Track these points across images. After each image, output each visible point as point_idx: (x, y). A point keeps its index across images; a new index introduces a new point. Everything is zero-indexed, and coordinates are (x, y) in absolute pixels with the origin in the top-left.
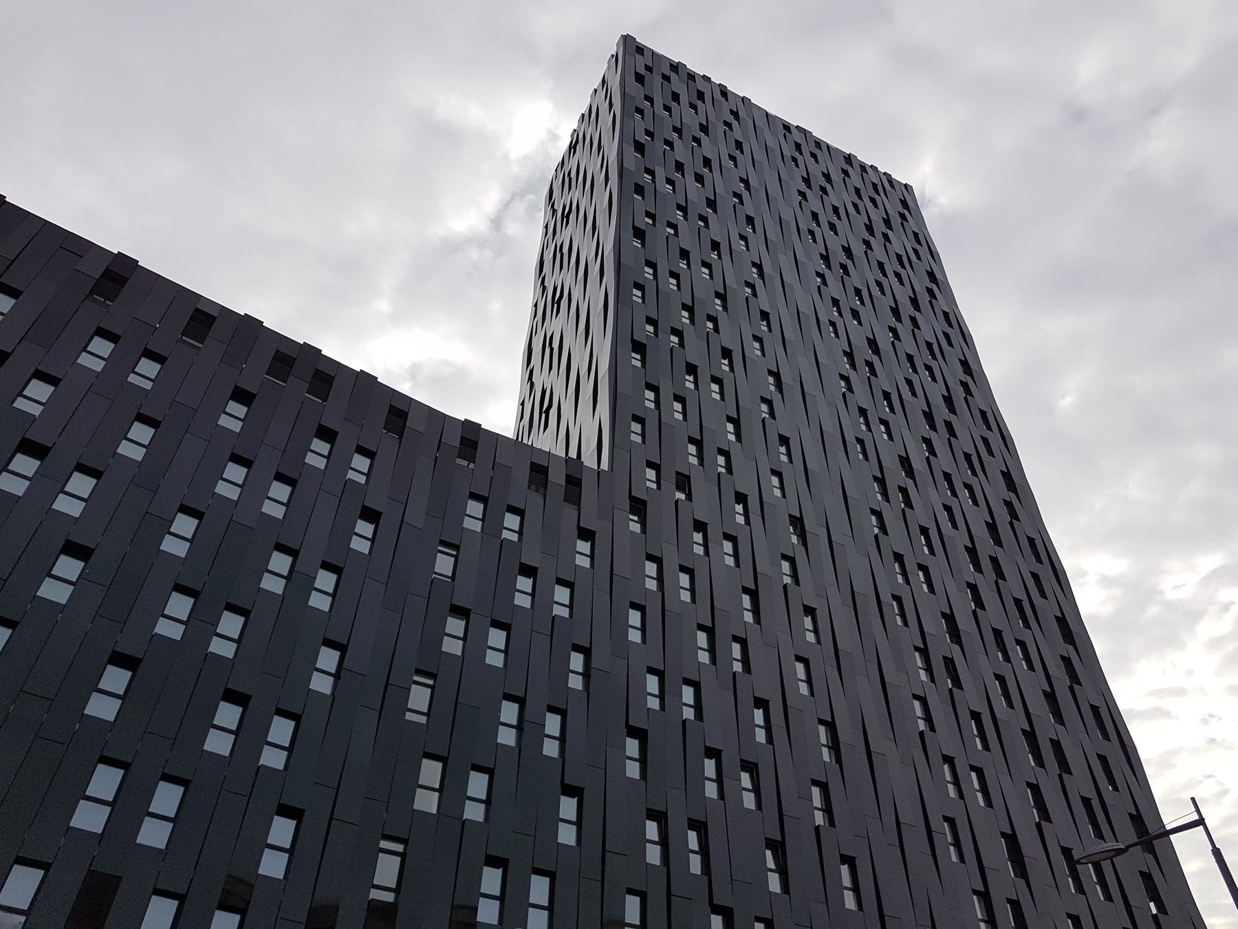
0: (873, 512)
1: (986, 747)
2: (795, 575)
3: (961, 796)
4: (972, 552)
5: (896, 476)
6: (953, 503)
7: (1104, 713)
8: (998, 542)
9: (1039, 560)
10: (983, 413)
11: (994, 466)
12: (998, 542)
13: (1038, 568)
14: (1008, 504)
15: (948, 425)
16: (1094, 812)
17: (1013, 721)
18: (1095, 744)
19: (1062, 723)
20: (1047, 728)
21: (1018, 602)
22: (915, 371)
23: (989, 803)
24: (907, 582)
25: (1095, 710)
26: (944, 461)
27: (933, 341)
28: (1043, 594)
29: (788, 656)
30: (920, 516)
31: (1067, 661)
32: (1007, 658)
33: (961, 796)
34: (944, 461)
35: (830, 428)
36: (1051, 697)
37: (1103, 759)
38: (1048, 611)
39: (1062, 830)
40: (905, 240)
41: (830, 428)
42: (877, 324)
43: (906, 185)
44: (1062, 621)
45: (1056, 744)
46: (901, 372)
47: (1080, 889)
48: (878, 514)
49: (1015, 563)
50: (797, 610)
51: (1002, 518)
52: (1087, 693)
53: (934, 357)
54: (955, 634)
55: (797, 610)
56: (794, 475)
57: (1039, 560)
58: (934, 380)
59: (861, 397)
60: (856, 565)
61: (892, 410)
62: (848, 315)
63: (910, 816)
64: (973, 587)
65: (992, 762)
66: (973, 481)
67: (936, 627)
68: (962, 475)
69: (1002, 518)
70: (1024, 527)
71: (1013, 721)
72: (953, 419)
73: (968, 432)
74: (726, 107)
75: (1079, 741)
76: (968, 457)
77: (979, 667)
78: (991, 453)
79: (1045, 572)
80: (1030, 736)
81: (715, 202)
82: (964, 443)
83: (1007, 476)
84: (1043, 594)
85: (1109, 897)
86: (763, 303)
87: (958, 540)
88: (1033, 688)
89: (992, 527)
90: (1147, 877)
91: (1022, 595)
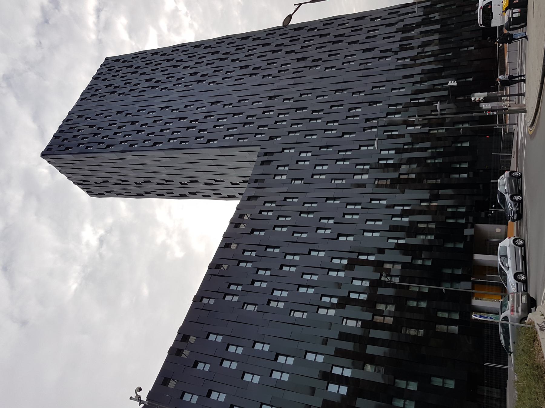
0: (161, 90)
3: (353, 61)
4: (133, 73)
6: (120, 76)
7: (218, 41)
9: (138, 57)
12: (172, 60)
13: (140, 58)
14: (123, 62)
18: (225, 45)
20: (220, 56)
22: (118, 75)
23: (355, 55)
24: (231, 77)
25: (217, 43)
30: (163, 78)
32: (253, 55)
35: (136, 99)
38: (192, 50)
39: (241, 56)
40: (178, 55)
41: (182, 94)
42: (137, 78)
43: (106, 60)
44: (195, 47)
46: (118, 79)
47: (311, 46)
49: (178, 56)
50: (214, 130)
51: (165, 57)
53: (113, 69)
56: (253, 99)
58: (121, 70)
59: (126, 90)
60: (174, 96)
63: (360, 73)
65: (343, 53)
66: (115, 70)
67: (193, 78)
70: (129, 59)
72: (221, 53)
73: (138, 63)
75: (334, 30)
76: (146, 64)
79: (182, 49)
80: (274, 52)
81: (370, 102)
82: (143, 64)
84: (188, 50)
89: (128, 67)
90: (309, 30)
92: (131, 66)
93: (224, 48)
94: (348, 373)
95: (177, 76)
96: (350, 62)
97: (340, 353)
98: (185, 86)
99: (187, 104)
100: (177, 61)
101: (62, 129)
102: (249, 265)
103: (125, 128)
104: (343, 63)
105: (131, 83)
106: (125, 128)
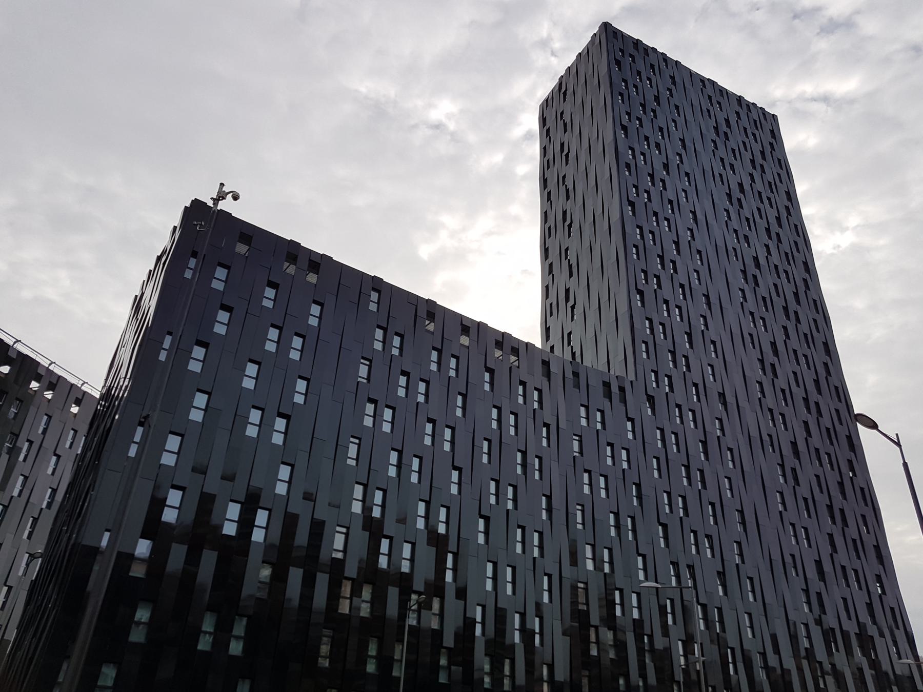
0: (725, 210)
1: (809, 516)
2: (706, 325)
3: (798, 543)
5: (736, 194)
7: (799, 227)
8: (780, 226)
9: (781, 168)
10: (779, 160)
11: (782, 188)
12: (780, 226)
15: (762, 166)
16: (857, 546)
17: (799, 393)
18: (834, 404)
19: (845, 499)
21: (786, 254)
22: (747, 137)
23: (810, 546)
26: (759, 185)
27: (772, 181)
28: (798, 251)
29: (705, 365)
30: (746, 212)
31: (805, 280)
33: (775, 426)
34: (759, 185)
35: (708, 168)
36: (817, 382)
37: (837, 411)
38: (799, 258)
41: (721, 244)
43: (773, 115)
45: (817, 404)
46: (740, 138)
47: (821, 465)
48: (727, 211)
50: (660, 301)
51: (801, 289)
52: (834, 380)
54: (776, 353)
55: (660, 301)
56: (704, 272)
57: (818, 312)
61: (735, 159)
62: (728, 167)
64: (767, 246)
65: (812, 525)
68: (802, 349)
69: (801, 289)
71: (799, 393)
73: (771, 169)
74: (667, 73)
75: (853, 508)
77: (786, 368)
78: (781, 182)
79: (820, 319)
80: (806, 400)
83: (772, 132)
85: (860, 588)
86: (686, 167)
87: (762, 224)
88: (789, 290)
89: (778, 219)
90: (850, 462)
91: (830, 426)
92: (764, 158)
93: (787, 234)
94: (258, 536)
95: (737, 165)
96: (795, 536)
97: (290, 522)
98: (735, 249)
99: (704, 254)
100: (778, 235)
101: (650, 52)
102: (434, 367)
103: (662, 162)
104: (793, 525)
105: (735, 159)
106: (662, 162)
